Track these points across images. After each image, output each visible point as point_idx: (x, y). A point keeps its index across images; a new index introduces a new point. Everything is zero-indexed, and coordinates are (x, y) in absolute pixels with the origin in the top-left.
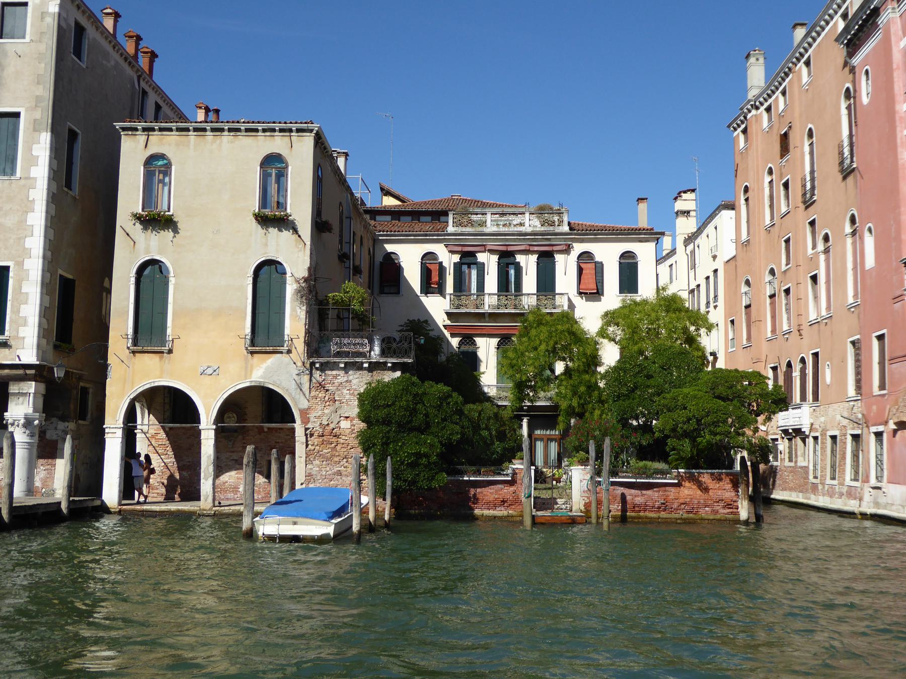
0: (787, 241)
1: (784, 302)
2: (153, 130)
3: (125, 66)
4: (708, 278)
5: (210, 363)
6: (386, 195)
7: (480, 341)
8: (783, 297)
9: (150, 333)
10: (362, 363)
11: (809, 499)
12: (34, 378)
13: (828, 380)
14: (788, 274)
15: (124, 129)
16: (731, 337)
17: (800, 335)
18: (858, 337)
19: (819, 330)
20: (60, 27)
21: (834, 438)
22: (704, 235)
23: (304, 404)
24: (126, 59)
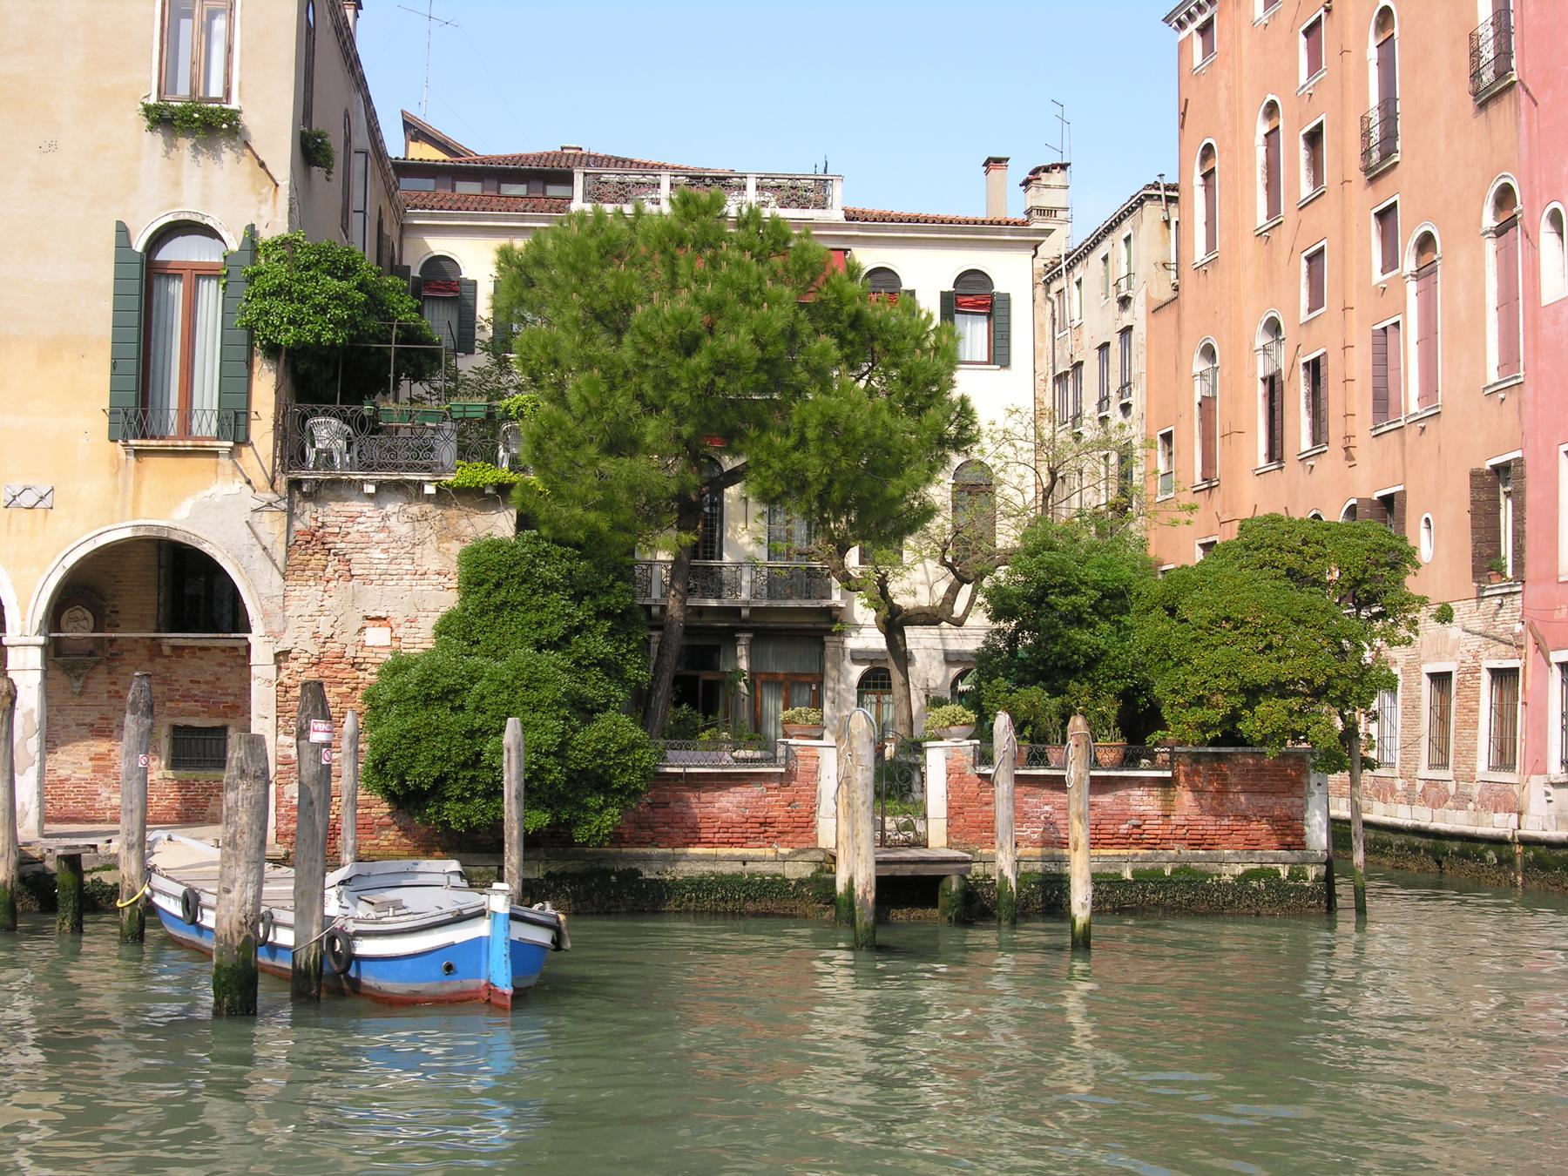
0: (1315, 258)
4: (1104, 347)
6: (415, 139)
10: (420, 485)
17: (1349, 457)
18: (1518, 454)
19: (1403, 445)
21: (1441, 680)
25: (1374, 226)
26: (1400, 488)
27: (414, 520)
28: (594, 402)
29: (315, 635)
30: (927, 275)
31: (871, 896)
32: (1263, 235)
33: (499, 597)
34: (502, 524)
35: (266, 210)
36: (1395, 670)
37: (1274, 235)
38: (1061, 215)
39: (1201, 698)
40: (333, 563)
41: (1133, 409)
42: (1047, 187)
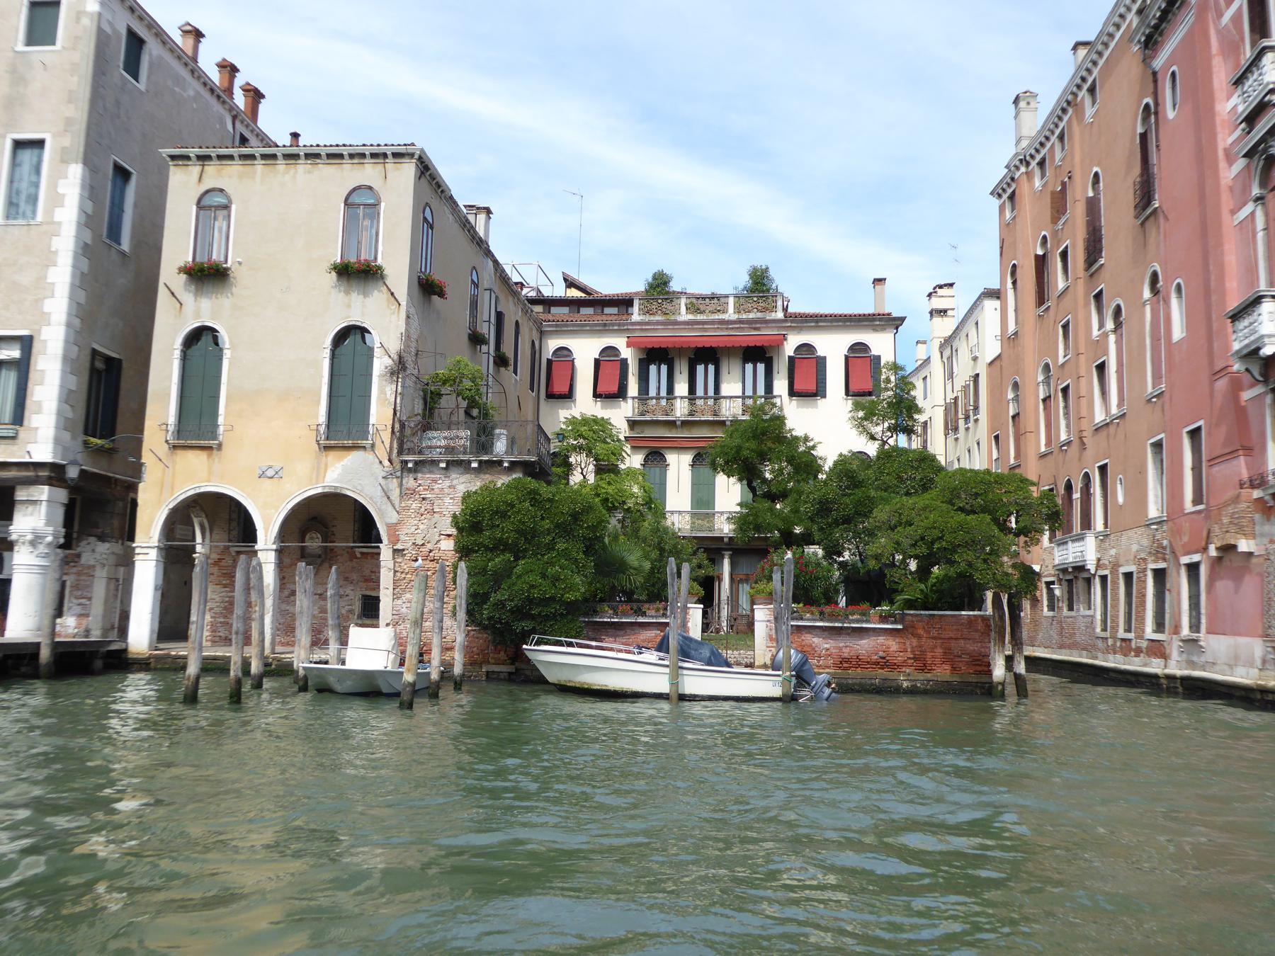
0: (1066, 327)
1: (1062, 404)
2: (208, 158)
3: (213, 101)
5: (271, 460)
7: (671, 458)
8: (1061, 399)
9: (197, 425)
10: (470, 462)
11: (1096, 658)
12: (50, 482)
13: (1121, 499)
14: (1066, 366)
15: (173, 157)
16: (995, 456)
20: (100, 31)
21: (1128, 576)
22: (963, 335)
23: (393, 517)
24: (212, 91)
38: (949, 313)
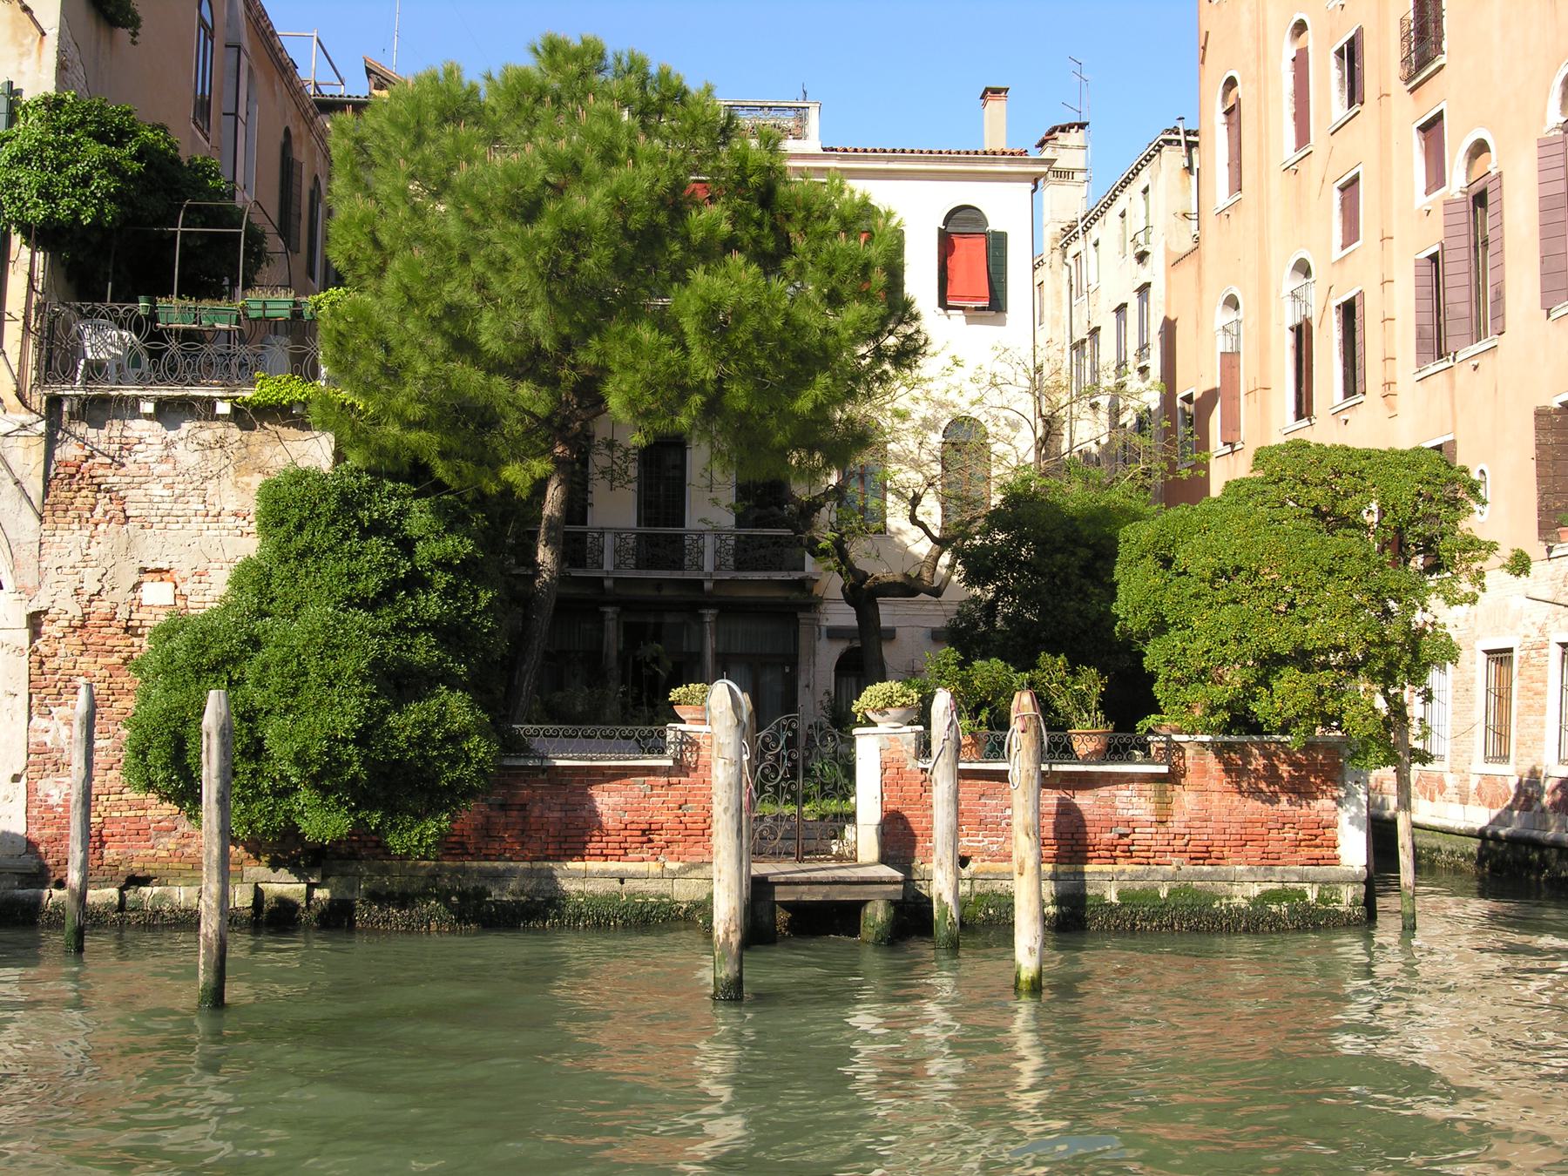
0: (1350, 187)
4: (1121, 309)
10: (210, 403)
19: (1452, 387)
21: (1500, 657)
25: (1416, 142)
26: (1450, 438)
27: (204, 447)
28: (418, 293)
29: (77, 593)
30: (915, 211)
31: (735, 939)
32: (1291, 169)
33: (300, 542)
34: (314, 451)
35: (29, 64)
36: (1323, 804)
37: (1301, 167)
39: (1204, 671)
40: (103, 499)
41: (1151, 372)
42: (1064, 147)
